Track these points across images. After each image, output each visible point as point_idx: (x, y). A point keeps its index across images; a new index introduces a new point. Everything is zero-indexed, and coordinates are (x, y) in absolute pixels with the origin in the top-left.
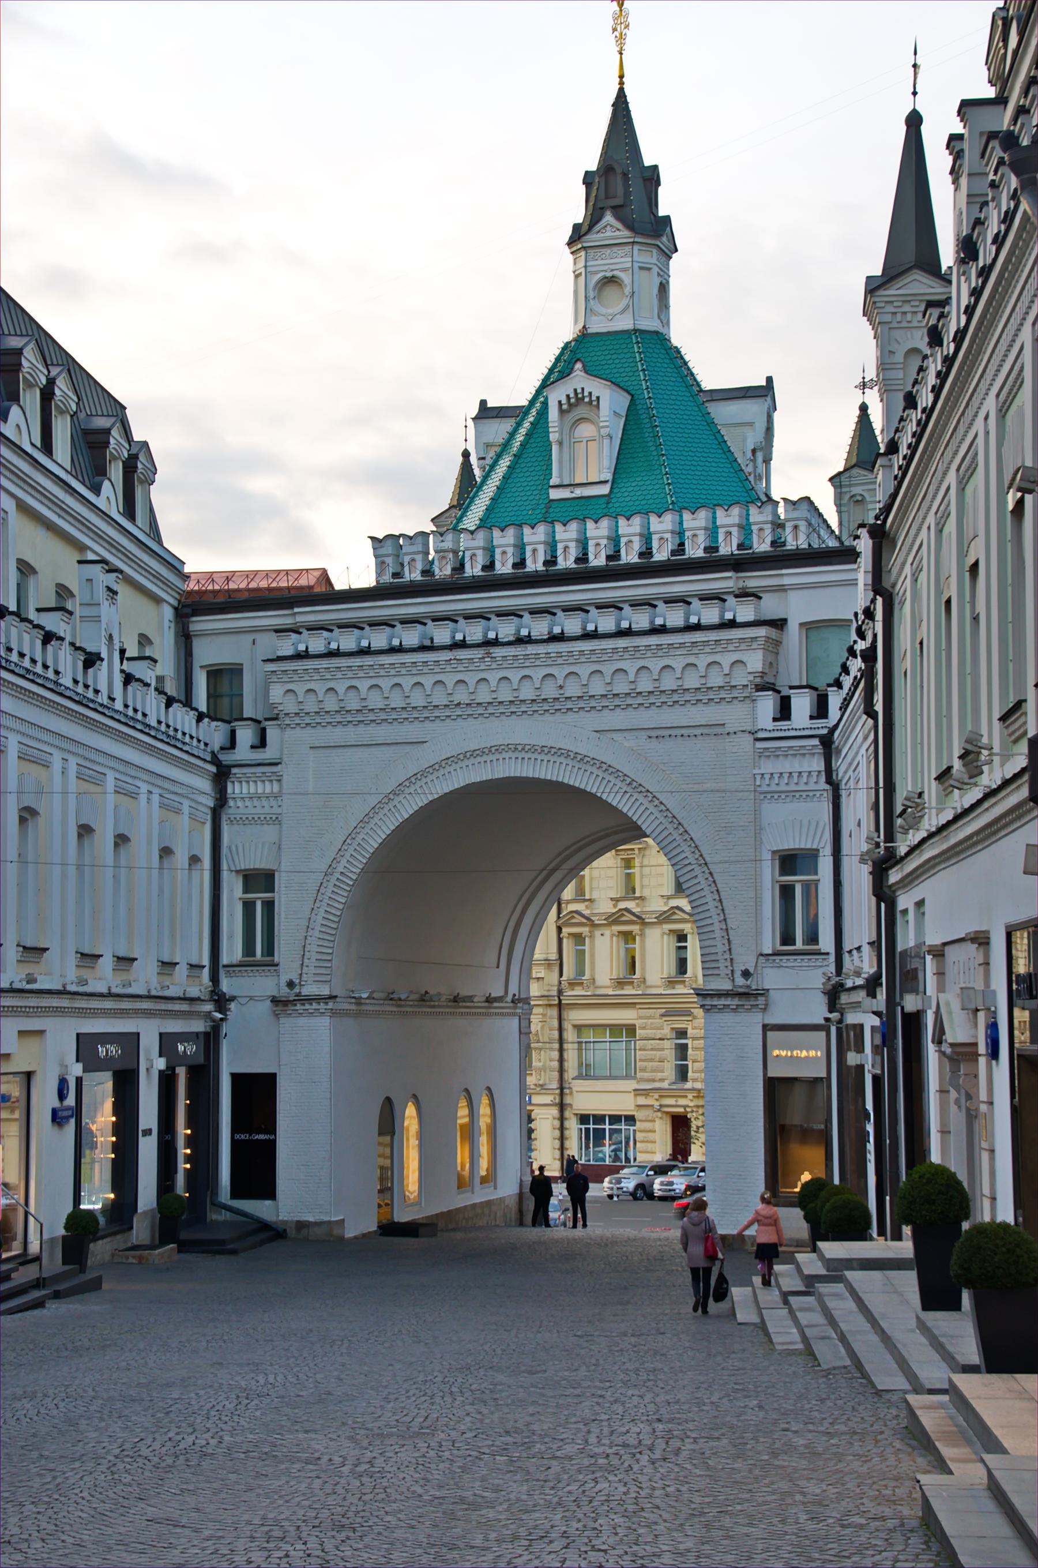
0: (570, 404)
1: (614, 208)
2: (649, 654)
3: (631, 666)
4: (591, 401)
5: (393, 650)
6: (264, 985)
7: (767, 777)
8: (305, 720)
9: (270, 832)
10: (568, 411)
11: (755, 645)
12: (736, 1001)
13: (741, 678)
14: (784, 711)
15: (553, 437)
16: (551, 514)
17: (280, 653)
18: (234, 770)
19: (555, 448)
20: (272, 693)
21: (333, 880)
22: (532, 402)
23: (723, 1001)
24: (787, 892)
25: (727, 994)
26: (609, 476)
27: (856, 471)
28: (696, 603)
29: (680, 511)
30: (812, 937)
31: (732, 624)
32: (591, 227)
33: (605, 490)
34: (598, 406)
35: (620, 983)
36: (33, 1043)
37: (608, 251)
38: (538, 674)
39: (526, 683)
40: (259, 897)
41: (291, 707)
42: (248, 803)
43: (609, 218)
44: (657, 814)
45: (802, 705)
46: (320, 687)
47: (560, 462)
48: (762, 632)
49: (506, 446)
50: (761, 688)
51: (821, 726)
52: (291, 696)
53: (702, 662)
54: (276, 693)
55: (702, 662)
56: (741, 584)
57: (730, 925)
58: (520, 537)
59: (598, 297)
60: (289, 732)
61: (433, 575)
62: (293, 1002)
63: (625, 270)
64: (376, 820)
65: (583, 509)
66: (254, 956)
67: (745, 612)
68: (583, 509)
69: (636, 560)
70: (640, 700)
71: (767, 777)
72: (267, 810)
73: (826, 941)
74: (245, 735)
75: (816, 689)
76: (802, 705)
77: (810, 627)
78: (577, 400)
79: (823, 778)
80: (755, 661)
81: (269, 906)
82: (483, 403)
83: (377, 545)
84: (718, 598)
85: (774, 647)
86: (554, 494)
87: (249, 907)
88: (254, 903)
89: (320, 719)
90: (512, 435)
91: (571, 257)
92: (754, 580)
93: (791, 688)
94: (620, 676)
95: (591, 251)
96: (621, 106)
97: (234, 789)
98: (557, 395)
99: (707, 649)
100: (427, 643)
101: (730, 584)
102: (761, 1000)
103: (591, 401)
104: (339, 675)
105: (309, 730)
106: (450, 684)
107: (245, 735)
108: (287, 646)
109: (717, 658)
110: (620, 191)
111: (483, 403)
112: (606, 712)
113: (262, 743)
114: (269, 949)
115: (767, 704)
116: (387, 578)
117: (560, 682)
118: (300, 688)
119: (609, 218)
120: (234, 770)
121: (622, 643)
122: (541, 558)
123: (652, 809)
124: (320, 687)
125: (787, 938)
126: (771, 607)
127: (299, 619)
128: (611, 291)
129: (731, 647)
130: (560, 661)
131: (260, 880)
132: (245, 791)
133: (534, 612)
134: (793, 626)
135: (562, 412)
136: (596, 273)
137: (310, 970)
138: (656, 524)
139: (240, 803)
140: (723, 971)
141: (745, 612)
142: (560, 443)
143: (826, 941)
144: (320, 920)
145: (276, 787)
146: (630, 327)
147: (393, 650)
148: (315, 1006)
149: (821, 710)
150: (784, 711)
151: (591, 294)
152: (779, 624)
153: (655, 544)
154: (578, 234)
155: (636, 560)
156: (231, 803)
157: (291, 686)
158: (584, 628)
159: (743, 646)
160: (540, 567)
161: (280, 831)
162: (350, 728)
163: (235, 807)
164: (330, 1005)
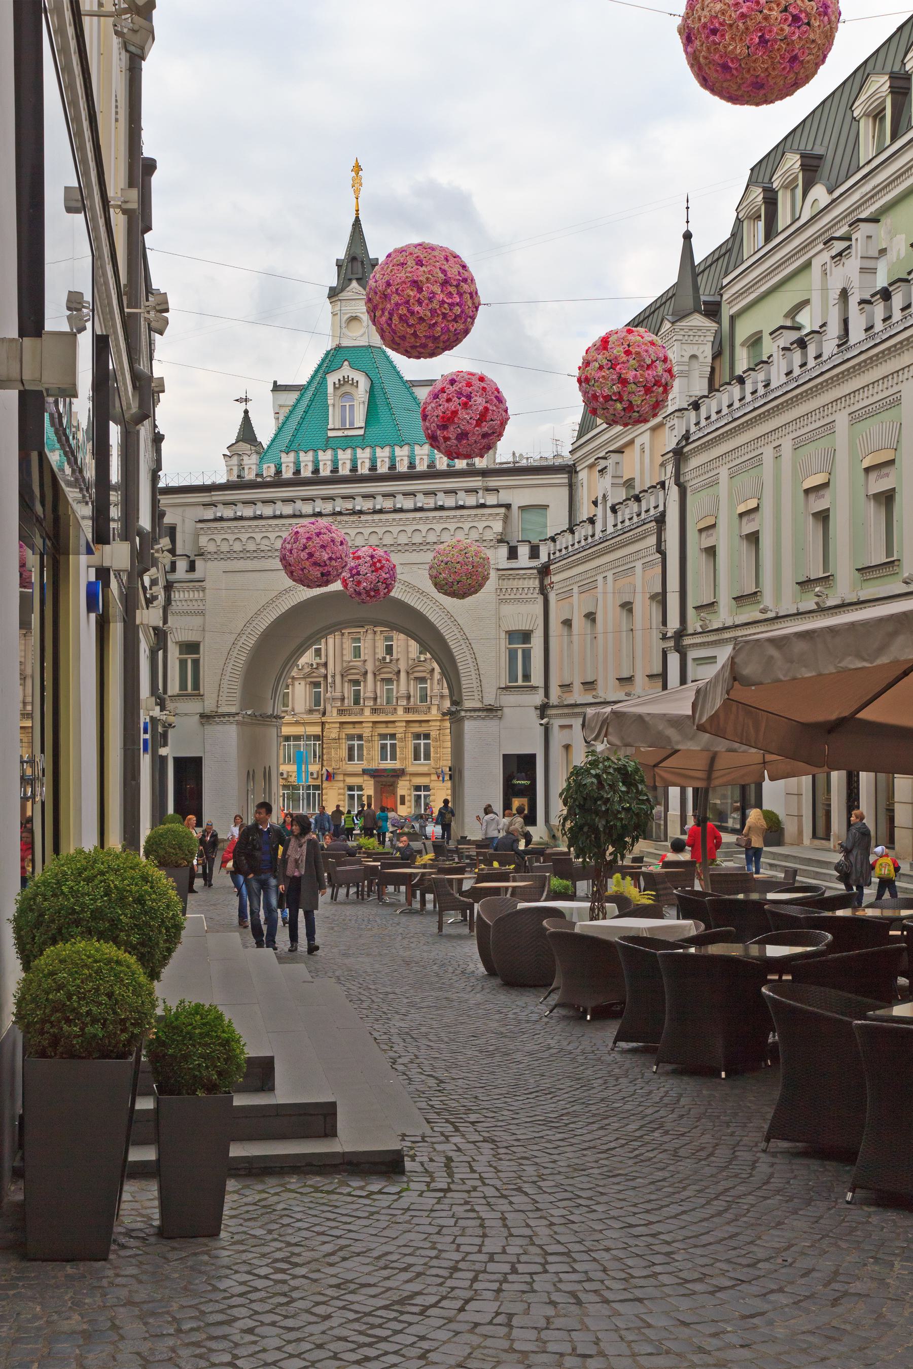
0: (340, 384)
1: (358, 280)
2: (435, 521)
3: (424, 528)
4: (352, 384)
5: (275, 517)
6: (194, 707)
7: (504, 590)
8: (219, 555)
9: (197, 621)
10: (338, 388)
11: (498, 518)
12: (485, 714)
13: (489, 535)
14: (513, 554)
15: (330, 402)
16: (328, 444)
17: (205, 518)
18: (175, 585)
19: (331, 409)
20: (200, 540)
21: (238, 647)
22: (309, 383)
23: (477, 714)
24: (512, 655)
25: (479, 710)
26: (363, 425)
27: (241, 443)
28: (279, 504)
29: (392, 446)
30: (527, 677)
31: (483, 506)
32: (342, 290)
33: (361, 432)
34: (357, 387)
35: (311, 711)
36: (566, 731)
37: (354, 302)
38: (367, 531)
39: (360, 536)
40: (189, 658)
41: (211, 548)
42: (184, 603)
43: (354, 284)
44: (438, 610)
45: (524, 551)
46: (231, 537)
47: (334, 416)
48: (502, 510)
49: (295, 406)
50: (500, 541)
51: (535, 563)
52: (212, 542)
53: (466, 526)
54: (203, 541)
55: (466, 526)
56: (485, 484)
57: (481, 672)
58: (413, 451)
59: (347, 327)
60: (209, 563)
61: (435, 466)
62: (213, 717)
63: (362, 313)
64: (265, 613)
65: (349, 443)
66: (186, 690)
67: (491, 500)
68: (349, 443)
69: (367, 472)
70: (428, 547)
71: (504, 590)
72: (196, 607)
73: (537, 679)
74: (182, 565)
75: (189, 557)
76: (524, 551)
77: (523, 508)
78: (345, 381)
79: (537, 590)
80: (498, 526)
81: (196, 663)
82: (275, 382)
83: (228, 459)
84: (475, 491)
85: (506, 519)
86: (330, 434)
87: (183, 663)
88: (186, 661)
89: (230, 555)
90: (298, 401)
91: (330, 306)
92: (493, 482)
93: (518, 541)
94: (417, 533)
95: (344, 303)
96: (357, 223)
97: (176, 596)
98: (332, 379)
99: (470, 519)
100: (298, 513)
101: (480, 484)
102: (499, 713)
103: (352, 384)
104: (243, 530)
105: (222, 562)
106: (244, 540)
107: (182, 565)
108: (209, 514)
109: (475, 524)
110: (360, 271)
111: (275, 382)
112: (407, 553)
113: (192, 568)
114: (196, 686)
115: (504, 551)
116: (234, 478)
117: (380, 536)
118: (218, 538)
119: (354, 284)
120: (175, 585)
121: (418, 515)
122: (329, 469)
123: (435, 608)
124: (231, 537)
125: (513, 678)
126: (504, 497)
127: (214, 498)
128: (354, 324)
129: (484, 518)
130: (380, 524)
131: (191, 648)
132: (191, 596)
133: (245, 503)
134: (515, 508)
135: (335, 388)
136: (346, 314)
137: (223, 698)
138: (398, 451)
139: (178, 603)
140: (477, 697)
141: (491, 500)
142: (334, 405)
143: (537, 679)
144: (229, 670)
145: (201, 594)
146: (367, 344)
147: (275, 517)
148: (227, 718)
149: (534, 553)
150: (513, 554)
151: (344, 325)
152: (508, 506)
153: (379, 464)
154: (333, 293)
155: (310, 475)
156: (173, 603)
157: (212, 537)
158: (255, 512)
159: (491, 518)
160: (348, 473)
161: (205, 619)
162: (248, 561)
163: (174, 606)
164: (237, 718)
